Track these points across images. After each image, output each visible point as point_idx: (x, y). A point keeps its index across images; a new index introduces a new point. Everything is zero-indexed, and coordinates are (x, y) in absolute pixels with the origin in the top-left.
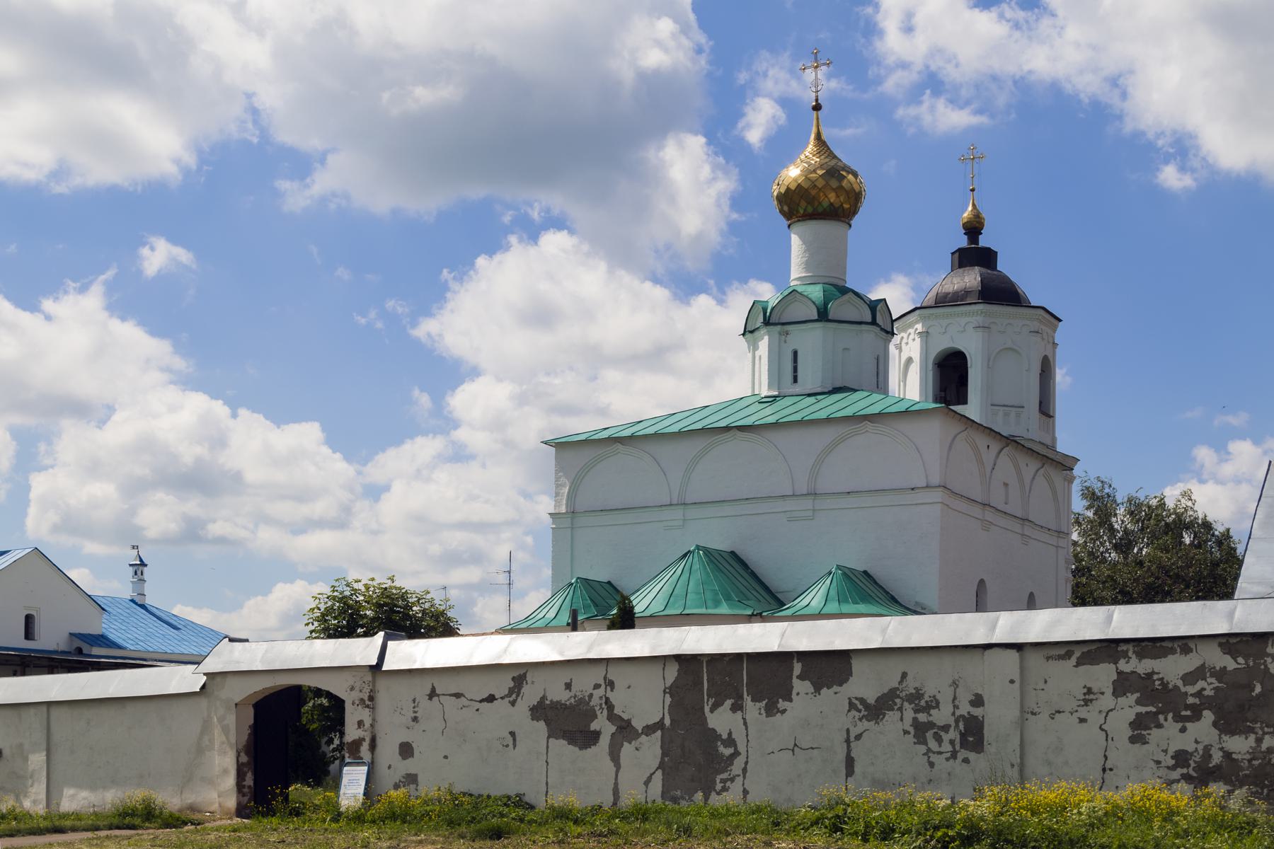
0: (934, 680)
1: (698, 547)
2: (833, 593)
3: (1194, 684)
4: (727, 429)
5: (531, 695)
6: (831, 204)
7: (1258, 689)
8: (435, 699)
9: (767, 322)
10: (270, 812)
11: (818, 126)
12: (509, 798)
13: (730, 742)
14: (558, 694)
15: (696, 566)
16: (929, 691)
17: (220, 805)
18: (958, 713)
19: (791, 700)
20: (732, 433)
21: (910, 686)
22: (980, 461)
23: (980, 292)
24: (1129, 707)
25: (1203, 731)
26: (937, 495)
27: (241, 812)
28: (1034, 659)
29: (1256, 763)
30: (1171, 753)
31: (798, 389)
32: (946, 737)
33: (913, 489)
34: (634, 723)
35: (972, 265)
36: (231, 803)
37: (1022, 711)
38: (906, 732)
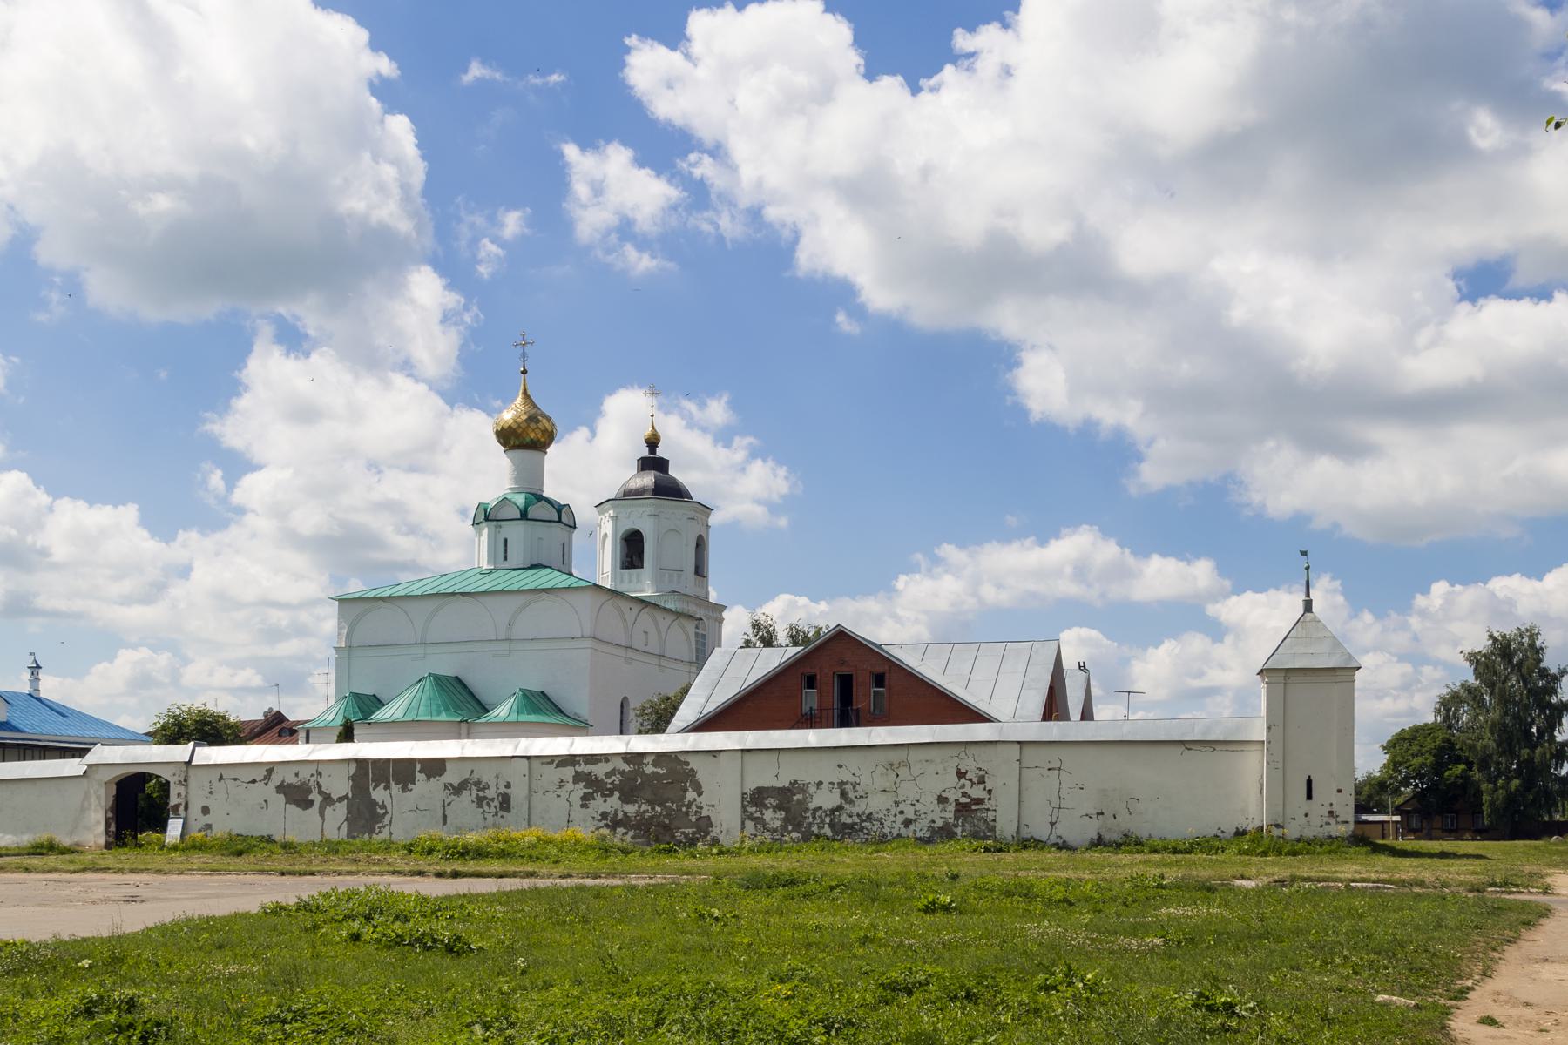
0: (487, 776)
1: (430, 674)
2: (515, 707)
3: (610, 777)
4: (453, 594)
5: (276, 780)
6: (532, 440)
7: (639, 781)
8: (222, 781)
9: (487, 519)
10: (125, 845)
11: (525, 385)
12: (263, 837)
13: (383, 806)
14: (291, 779)
15: (427, 687)
16: (484, 780)
17: (95, 842)
18: (499, 792)
19: (415, 784)
20: (454, 598)
21: (475, 777)
22: (624, 619)
23: (654, 490)
24: (580, 789)
25: (614, 802)
26: (588, 643)
27: (108, 846)
28: (536, 764)
29: (638, 818)
30: (599, 813)
31: (507, 565)
32: (492, 804)
33: (573, 638)
34: (332, 796)
35: (650, 469)
36: (102, 841)
37: (530, 791)
38: (473, 802)
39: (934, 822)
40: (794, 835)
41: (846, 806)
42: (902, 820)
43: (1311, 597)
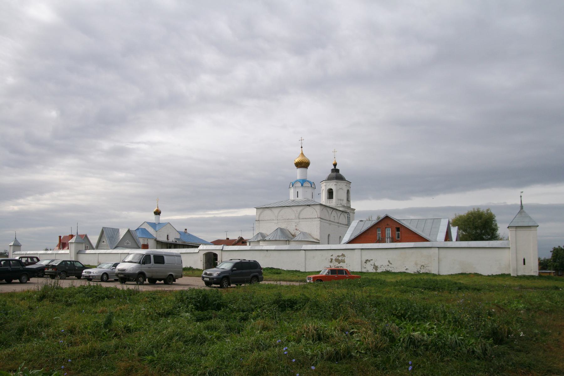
22: (328, 212)
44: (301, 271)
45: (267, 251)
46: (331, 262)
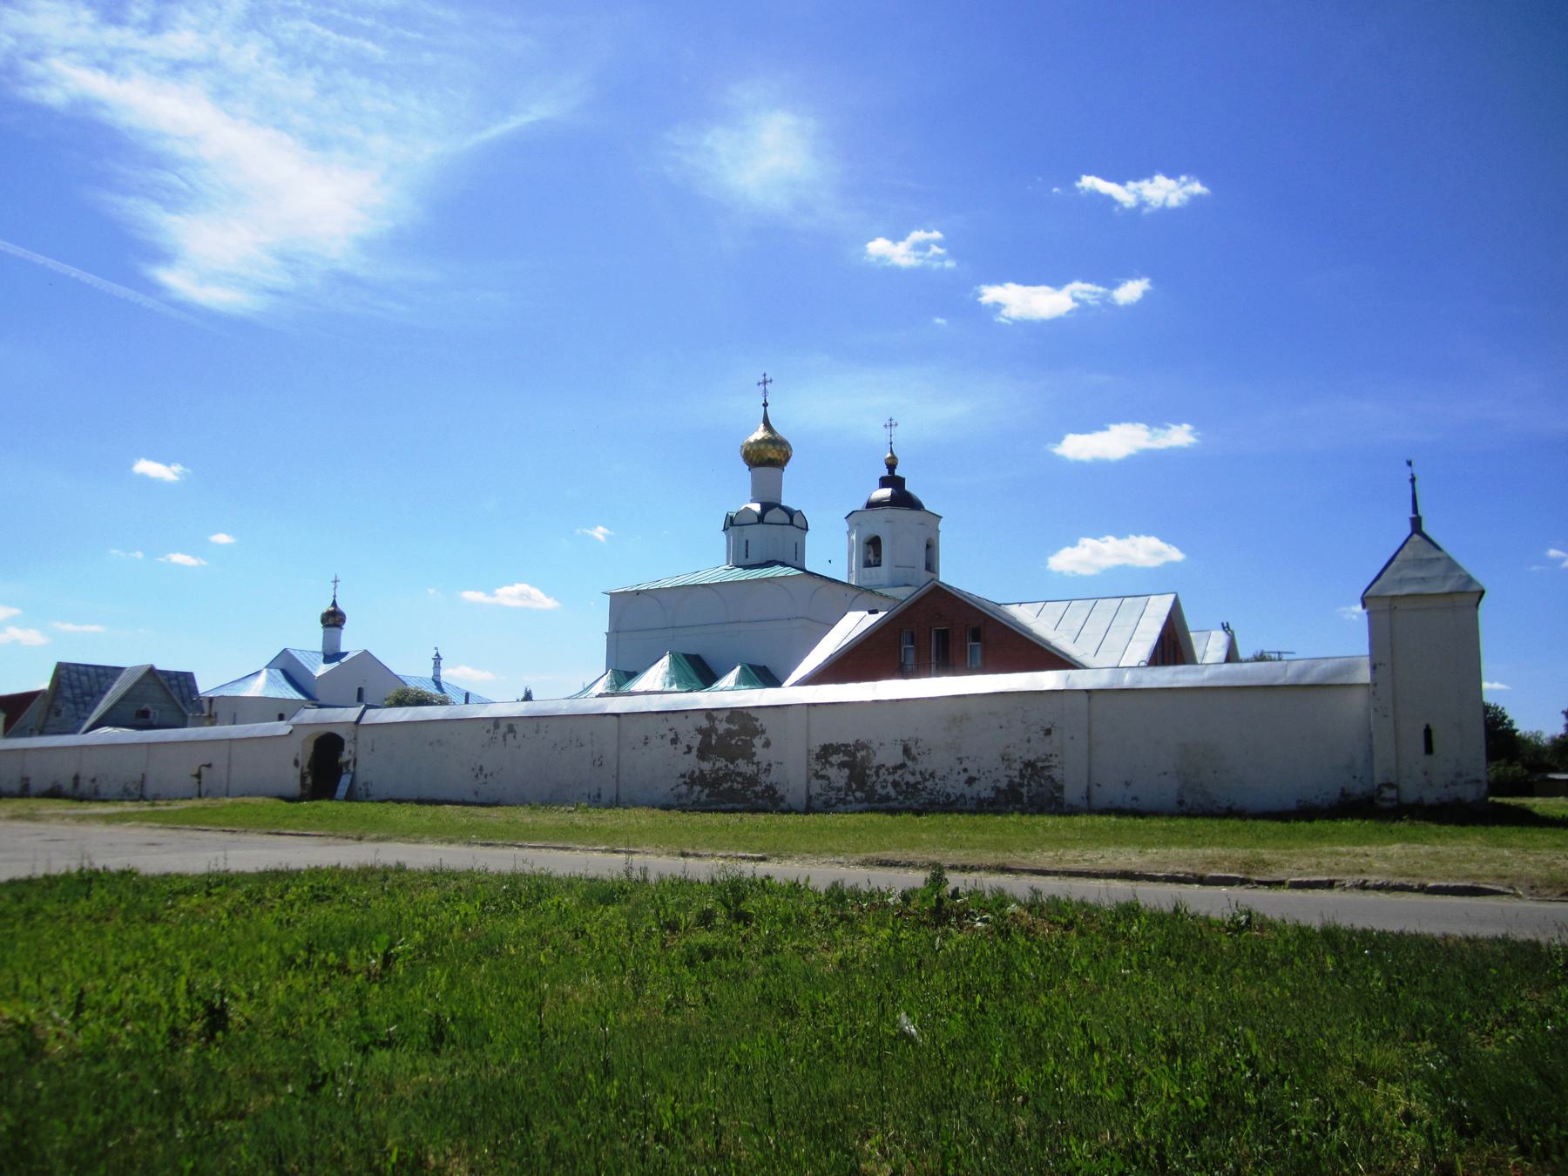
39: (998, 781)
40: (858, 794)
41: (909, 763)
42: (966, 778)
43: (1420, 513)
44: (408, 866)
45: (1262, 653)
46: (671, 730)
